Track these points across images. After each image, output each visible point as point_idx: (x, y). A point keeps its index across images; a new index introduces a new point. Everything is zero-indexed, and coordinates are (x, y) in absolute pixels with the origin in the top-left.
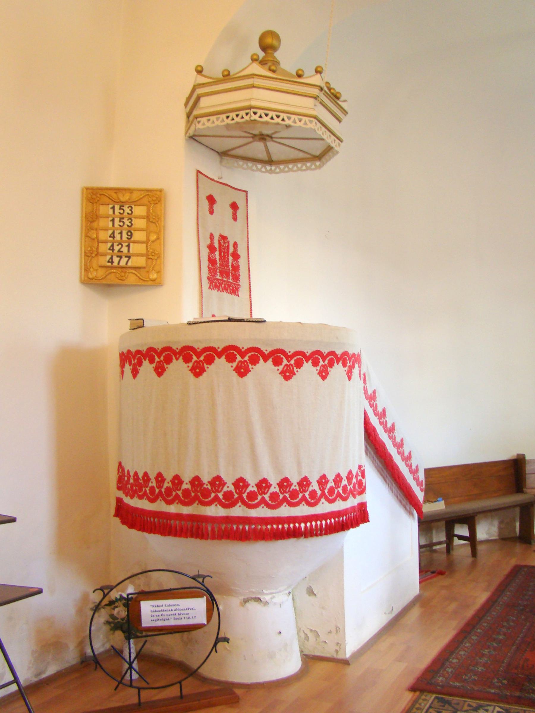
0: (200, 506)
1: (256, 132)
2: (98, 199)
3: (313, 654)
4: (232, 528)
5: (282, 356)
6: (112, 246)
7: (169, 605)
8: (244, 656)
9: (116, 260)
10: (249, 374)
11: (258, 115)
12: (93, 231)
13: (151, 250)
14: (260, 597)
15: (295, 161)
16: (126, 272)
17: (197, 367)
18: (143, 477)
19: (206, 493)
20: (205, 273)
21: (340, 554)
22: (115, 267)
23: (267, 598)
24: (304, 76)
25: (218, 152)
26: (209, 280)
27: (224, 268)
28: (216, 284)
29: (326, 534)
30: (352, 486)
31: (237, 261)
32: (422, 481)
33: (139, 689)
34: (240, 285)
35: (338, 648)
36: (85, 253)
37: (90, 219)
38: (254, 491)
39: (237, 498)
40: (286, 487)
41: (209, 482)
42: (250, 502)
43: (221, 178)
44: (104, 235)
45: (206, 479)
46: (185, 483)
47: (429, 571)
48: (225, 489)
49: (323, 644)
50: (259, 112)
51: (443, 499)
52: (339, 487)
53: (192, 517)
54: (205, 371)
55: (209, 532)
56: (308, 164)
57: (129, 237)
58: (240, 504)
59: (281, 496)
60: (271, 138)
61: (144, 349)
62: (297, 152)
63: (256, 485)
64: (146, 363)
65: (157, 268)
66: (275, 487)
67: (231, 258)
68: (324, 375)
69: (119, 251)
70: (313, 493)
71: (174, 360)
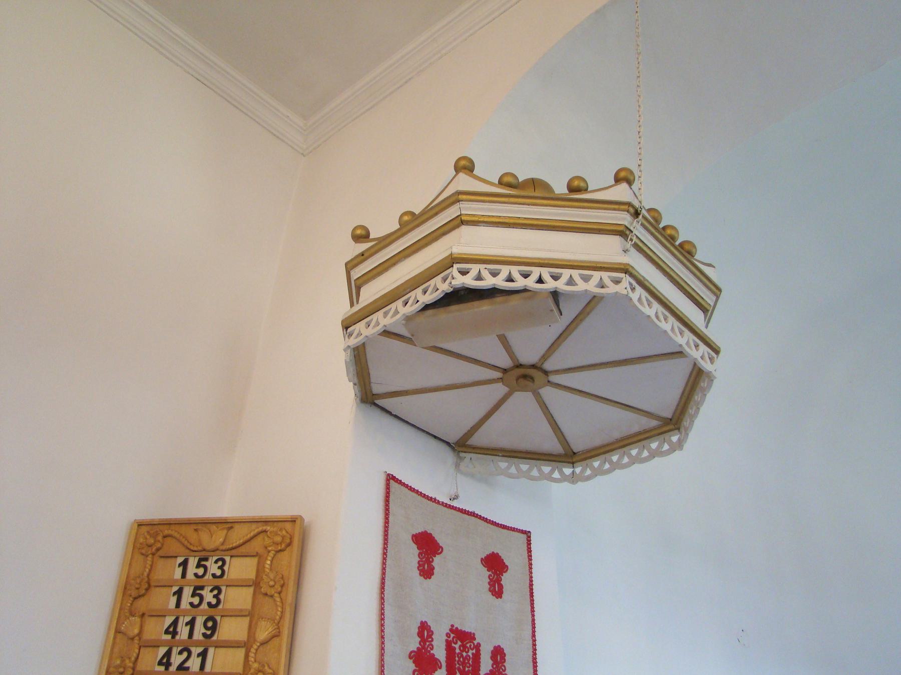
2: (159, 545)
6: (168, 654)
13: (256, 665)
25: (448, 443)
37: (134, 592)
43: (456, 497)
57: (209, 632)
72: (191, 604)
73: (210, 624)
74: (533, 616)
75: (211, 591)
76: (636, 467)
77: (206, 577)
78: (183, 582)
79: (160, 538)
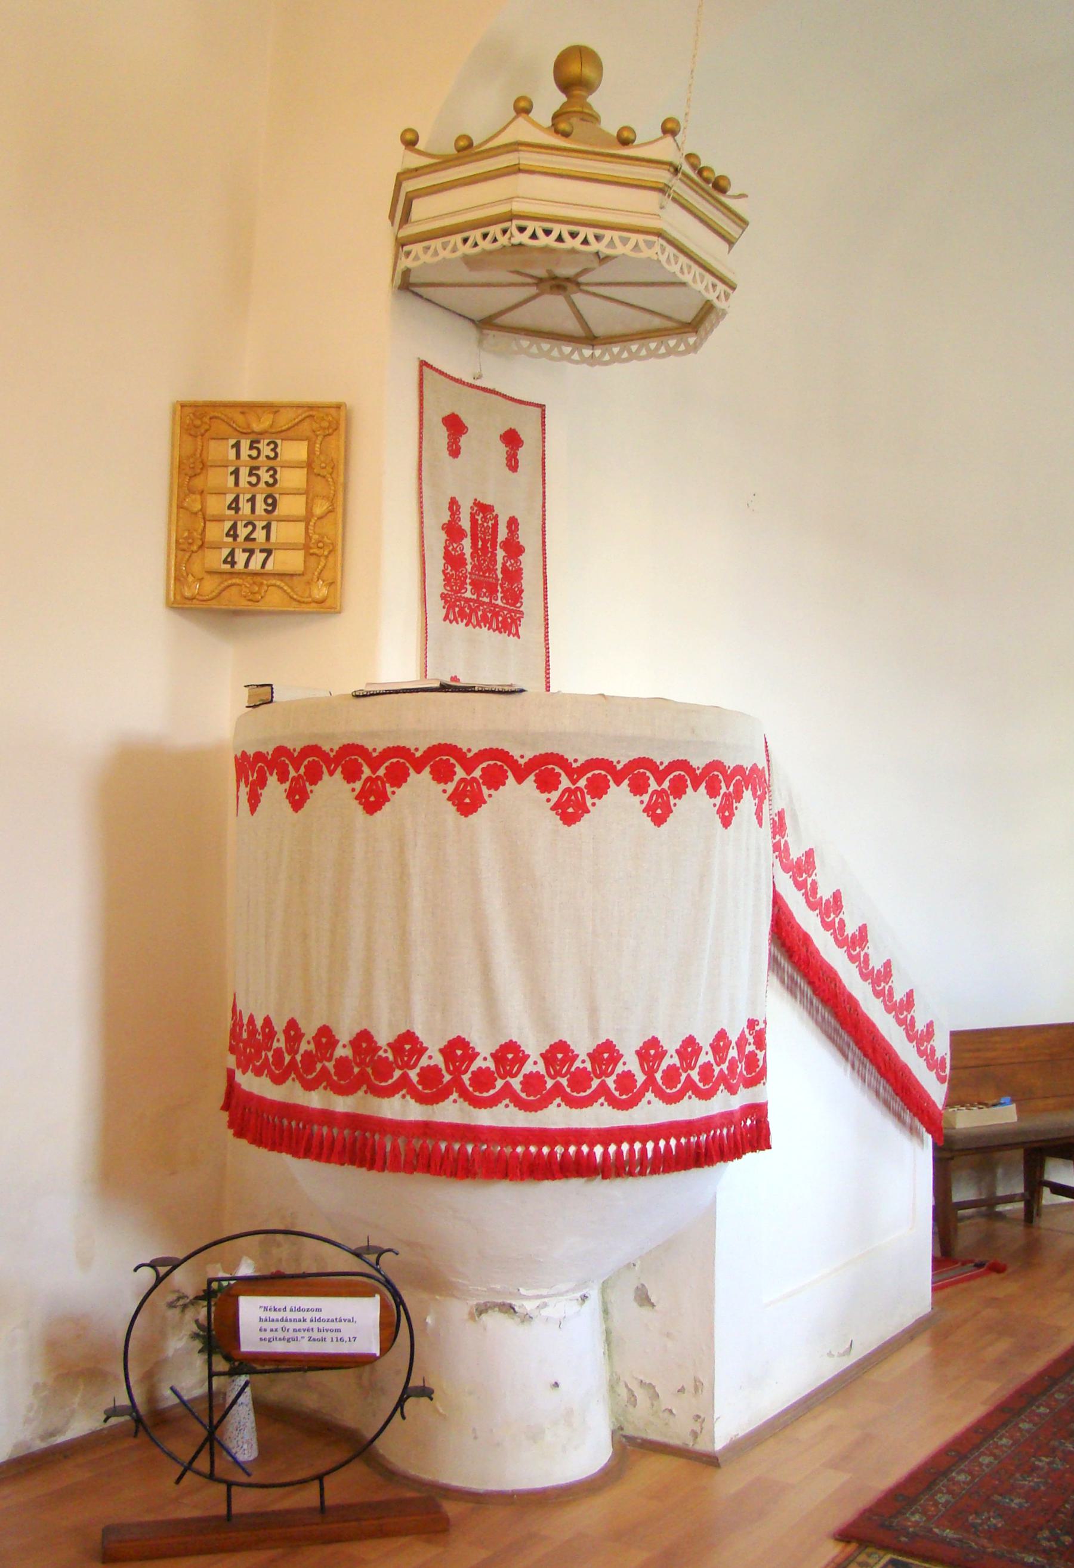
0: (370, 1096)
1: (541, 273)
2: (207, 427)
3: (644, 1435)
4: (436, 1147)
5: (557, 770)
6: (234, 527)
7: (299, 1310)
8: (474, 1429)
9: (241, 557)
10: (483, 810)
11: (529, 232)
12: (193, 497)
13: (316, 537)
14: (513, 1302)
15: (644, 335)
16: (262, 584)
17: (371, 792)
18: (263, 1028)
19: (383, 1069)
20: (436, 584)
21: (708, 1217)
22: (239, 574)
23: (529, 1306)
24: (636, 143)
25: (472, 321)
26: (446, 602)
27: (485, 572)
28: (462, 609)
29: (654, 1172)
30: (724, 1066)
31: (517, 561)
32: (943, 1059)
33: (230, 1485)
34: (522, 613)
35: (697, 1429)
36: (177, 541)
37: (189, 472)
38: (488, 1068)
39: (449, 1082)
40: (563, 1062)
41: (389, 1045)
42: (477, 1094)
43: (480, 377)
44: (217, 505)
45: (384, 1037)
46: (340, 1044)
47: (971, 1261)
48: (424, 1062)
49: (666, 1414)
50: (531, 226)
51: (1012, 1101)
52: (693, 1069)
53: (354, 1121)
54: (389, 800)
55: (388, 1155)
56: (672, 343)
57: (270, 508)
58: (455, 1096)
59: (550, 1083)
60: (578, 284)
61: (268, 749)
62: (647, 317)
63: (492, 1055)
64: (272, 780)
65: (327, 575)
66: (535, 1063)
67: (500, 554)
68: (658, 813)
69: (248, 538)
70: (628, 1076)
71: (326, 776)
72: (249, 483)
73: (270, 501)
74: (544, 488)
75: (267, 471)
76: (652, 361)
77: (260, 459)
78: (238, 463)
79: (206, 419)
